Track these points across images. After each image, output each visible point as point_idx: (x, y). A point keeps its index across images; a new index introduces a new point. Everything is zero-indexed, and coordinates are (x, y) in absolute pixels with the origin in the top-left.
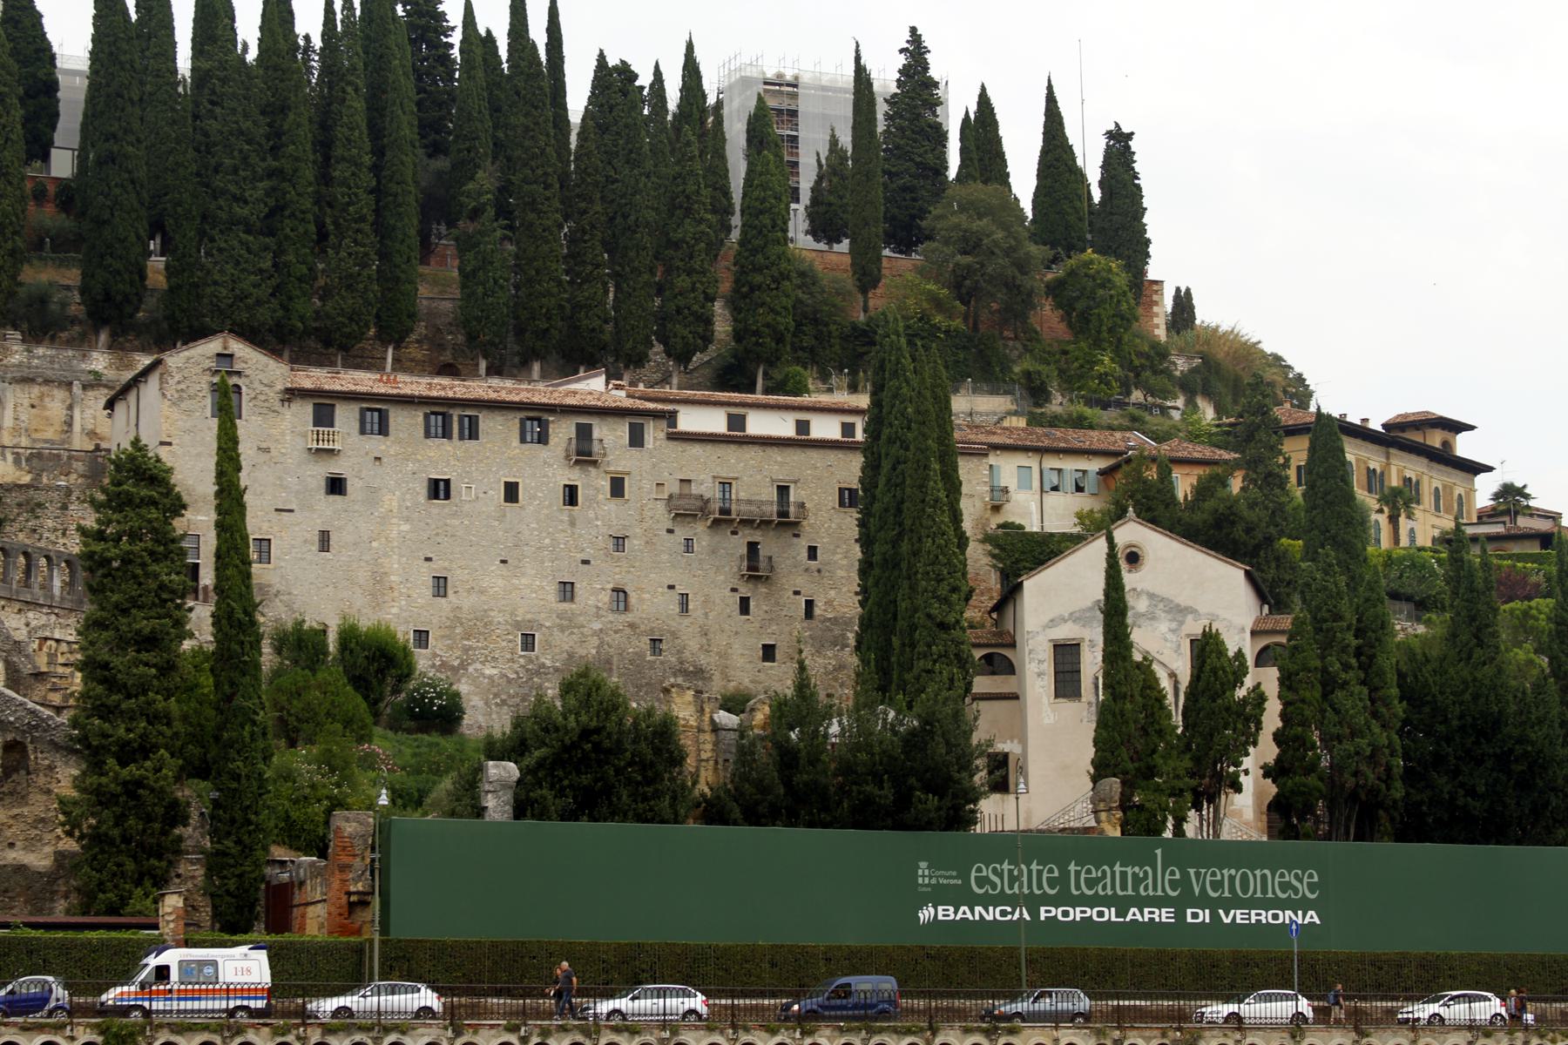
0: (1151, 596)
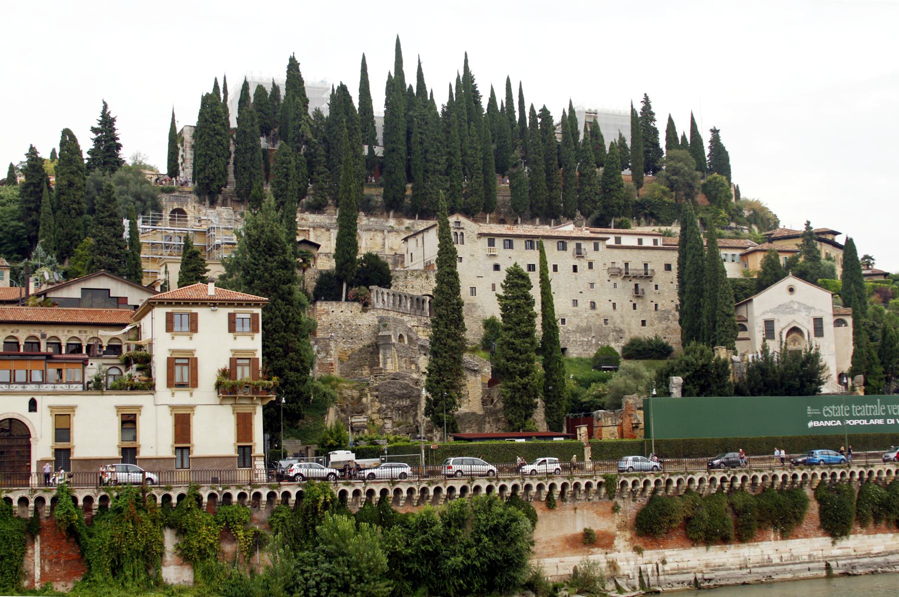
0: (799, 303)
